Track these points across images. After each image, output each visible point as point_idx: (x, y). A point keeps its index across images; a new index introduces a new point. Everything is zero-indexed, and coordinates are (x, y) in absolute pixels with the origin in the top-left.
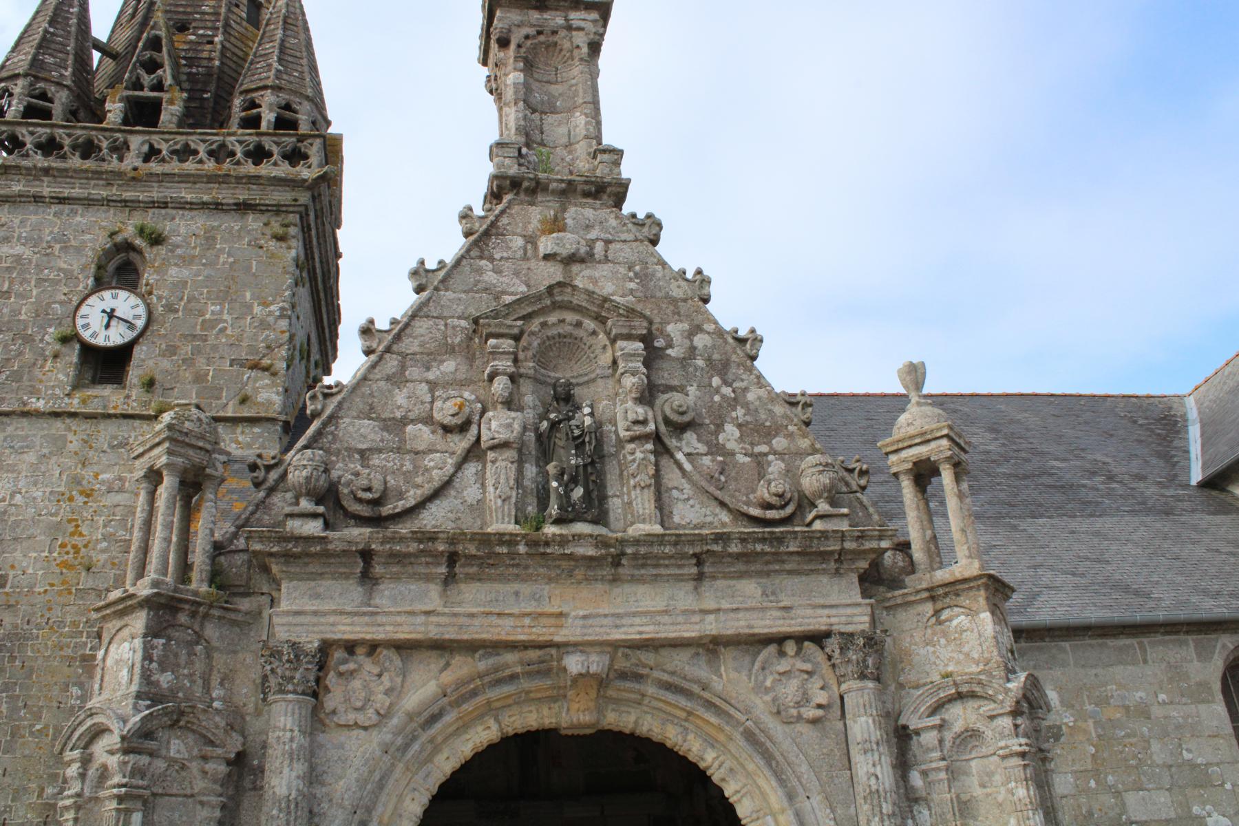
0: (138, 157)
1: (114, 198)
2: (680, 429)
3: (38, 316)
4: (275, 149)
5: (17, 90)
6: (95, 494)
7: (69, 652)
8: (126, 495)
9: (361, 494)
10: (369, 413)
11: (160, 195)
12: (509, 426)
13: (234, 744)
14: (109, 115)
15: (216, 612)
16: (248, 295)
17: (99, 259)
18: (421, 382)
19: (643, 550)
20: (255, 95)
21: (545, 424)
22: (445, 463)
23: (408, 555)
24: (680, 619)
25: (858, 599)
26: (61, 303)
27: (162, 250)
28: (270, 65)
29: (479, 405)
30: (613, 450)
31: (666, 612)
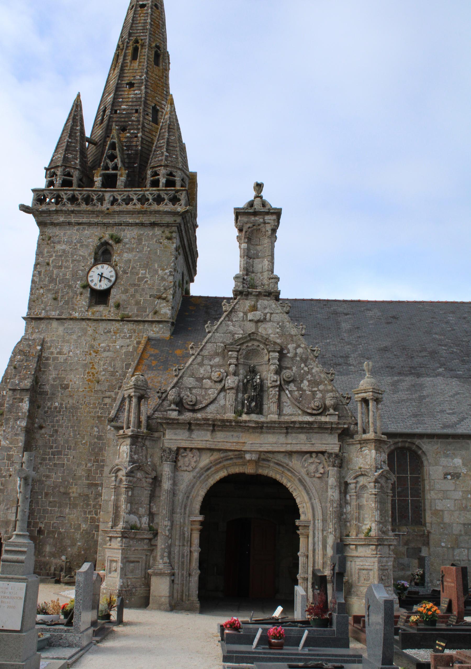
0: (109, 203)
1: (100, 222)
2: (288, 383)
3: (73, 276)
4: (166, 197)
5: (59, 173)
6: (99, 352)
7: (93, 414)
8: (111, 353)
9: (189, 403)
10: (192, 376)
11: (119, 220)
12: (234, 382)
13: (154, 474)
14: (96, 183)
15: (148, 438)
16: (156, 266)
17: (95, 250)
18: (208, 365)
19: (269, 425)
20: (156, 169)
21: (245, 381)
22: (214, 392)
23: (201, 424)
24: (280, 445)
25: (337, 442)
26: (82, 270)
27: (120, 245)
28: (162, 153)
29: (226, 374)
30: (266, 389)
31: (275, 443)
